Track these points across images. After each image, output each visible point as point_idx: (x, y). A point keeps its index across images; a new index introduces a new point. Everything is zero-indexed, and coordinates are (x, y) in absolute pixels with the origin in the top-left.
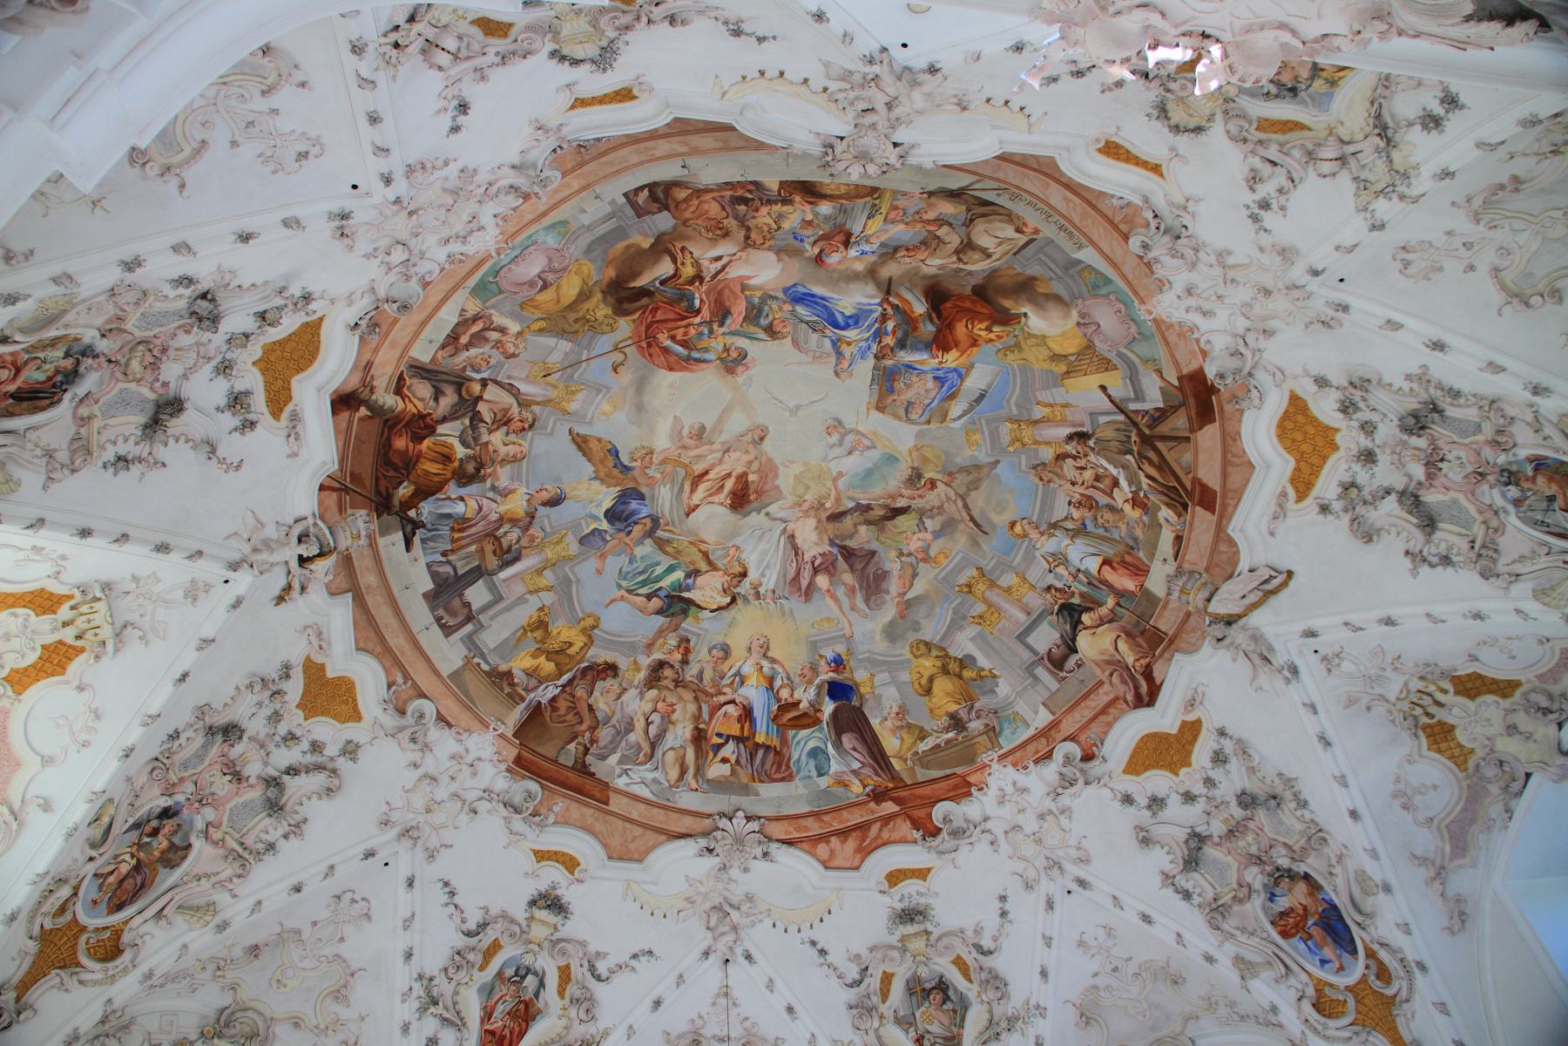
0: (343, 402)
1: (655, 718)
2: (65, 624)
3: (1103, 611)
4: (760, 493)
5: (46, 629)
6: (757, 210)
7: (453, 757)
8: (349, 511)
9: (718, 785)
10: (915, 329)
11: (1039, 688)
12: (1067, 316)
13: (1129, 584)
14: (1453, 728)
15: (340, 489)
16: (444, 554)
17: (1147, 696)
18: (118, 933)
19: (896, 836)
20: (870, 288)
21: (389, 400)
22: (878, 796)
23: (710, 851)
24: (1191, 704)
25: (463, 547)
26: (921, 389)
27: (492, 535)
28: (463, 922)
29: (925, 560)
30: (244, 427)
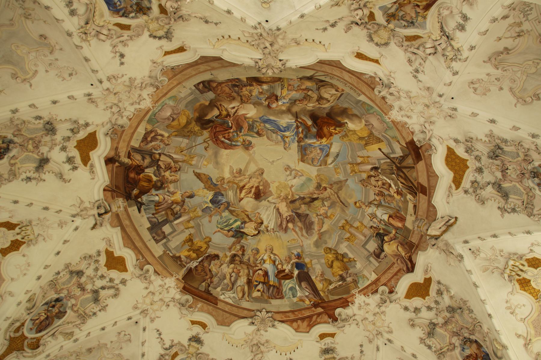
0: (109, 161)
1: (233, 274)
2: (18, 234)
3: (392, 235)
4: (265, 193)
5: (11, 236)
6: (242, 89)
7: (160, 286)
8: (116, 198)
9: (256, 300)
10: (309, 131)
11: (371, 265)
12: (361, 122)
13: (400, 225)
14: (530, 281)
15: (112, 190)
16: (153, 214)
17: (411, 269)
18: (38, 340)
19: (322, 320)
20: (290, 116)
21: (126, 160)
22: (315, 305)
23: (253, 323)
24: (426, 271)
25: (159, 212)
26: (315, 153)
27: (170, 208)
28: (164, 344)
29: (326, 217)
30: (73, 168)
